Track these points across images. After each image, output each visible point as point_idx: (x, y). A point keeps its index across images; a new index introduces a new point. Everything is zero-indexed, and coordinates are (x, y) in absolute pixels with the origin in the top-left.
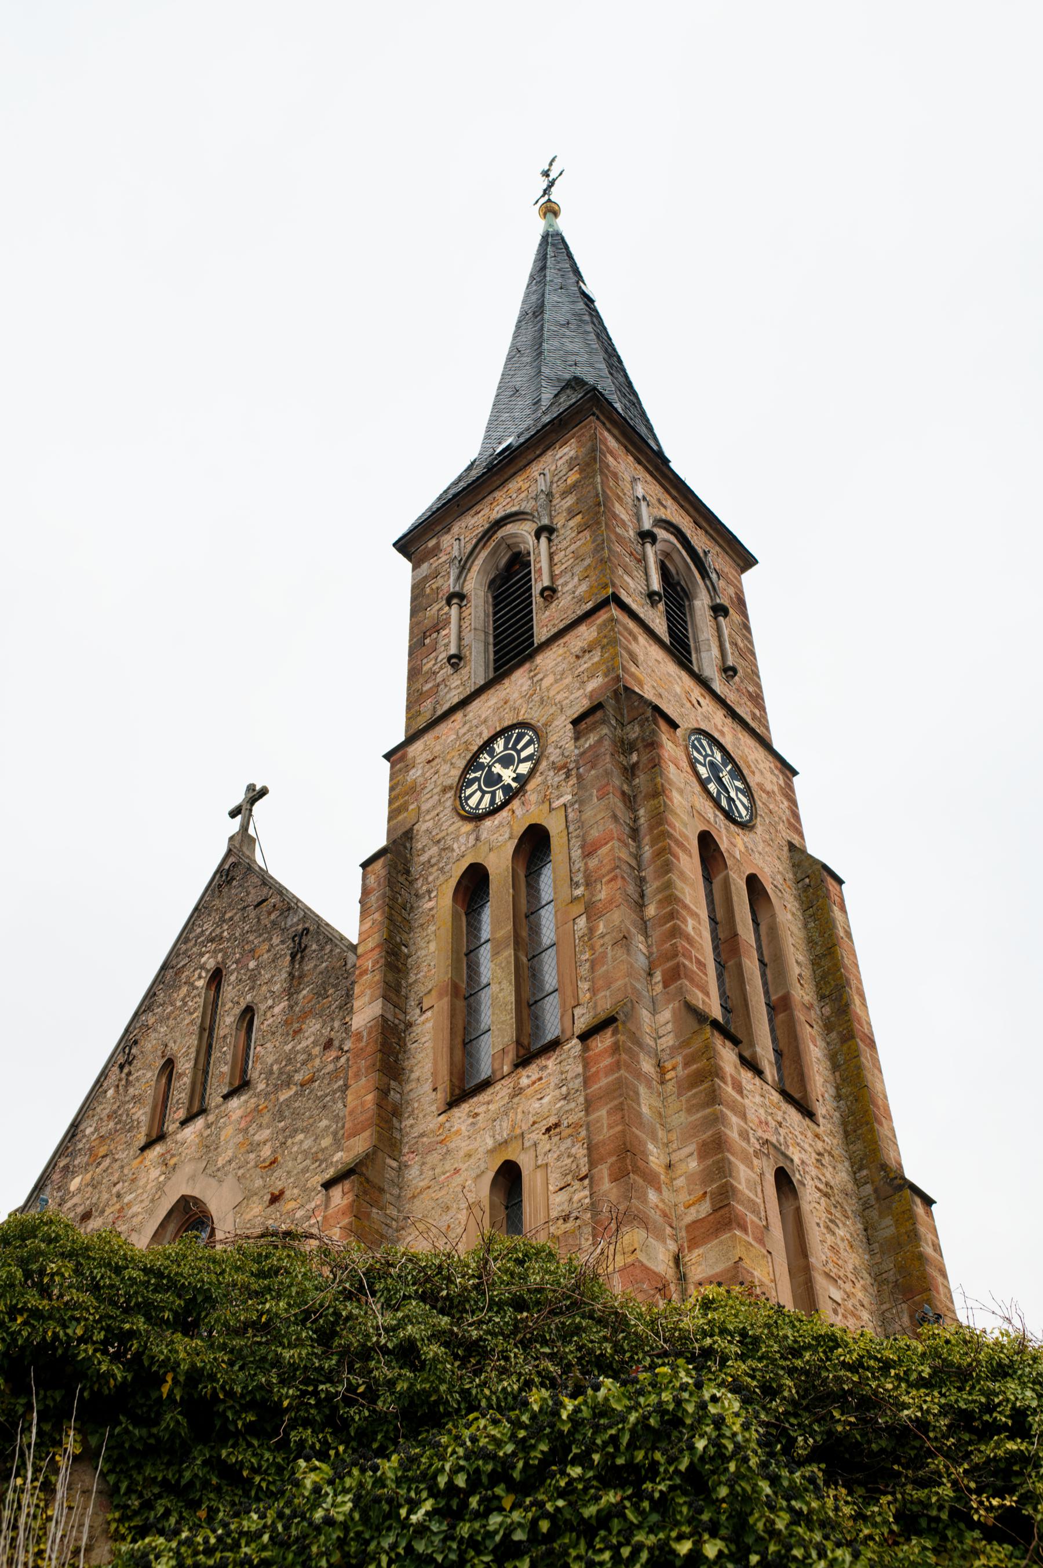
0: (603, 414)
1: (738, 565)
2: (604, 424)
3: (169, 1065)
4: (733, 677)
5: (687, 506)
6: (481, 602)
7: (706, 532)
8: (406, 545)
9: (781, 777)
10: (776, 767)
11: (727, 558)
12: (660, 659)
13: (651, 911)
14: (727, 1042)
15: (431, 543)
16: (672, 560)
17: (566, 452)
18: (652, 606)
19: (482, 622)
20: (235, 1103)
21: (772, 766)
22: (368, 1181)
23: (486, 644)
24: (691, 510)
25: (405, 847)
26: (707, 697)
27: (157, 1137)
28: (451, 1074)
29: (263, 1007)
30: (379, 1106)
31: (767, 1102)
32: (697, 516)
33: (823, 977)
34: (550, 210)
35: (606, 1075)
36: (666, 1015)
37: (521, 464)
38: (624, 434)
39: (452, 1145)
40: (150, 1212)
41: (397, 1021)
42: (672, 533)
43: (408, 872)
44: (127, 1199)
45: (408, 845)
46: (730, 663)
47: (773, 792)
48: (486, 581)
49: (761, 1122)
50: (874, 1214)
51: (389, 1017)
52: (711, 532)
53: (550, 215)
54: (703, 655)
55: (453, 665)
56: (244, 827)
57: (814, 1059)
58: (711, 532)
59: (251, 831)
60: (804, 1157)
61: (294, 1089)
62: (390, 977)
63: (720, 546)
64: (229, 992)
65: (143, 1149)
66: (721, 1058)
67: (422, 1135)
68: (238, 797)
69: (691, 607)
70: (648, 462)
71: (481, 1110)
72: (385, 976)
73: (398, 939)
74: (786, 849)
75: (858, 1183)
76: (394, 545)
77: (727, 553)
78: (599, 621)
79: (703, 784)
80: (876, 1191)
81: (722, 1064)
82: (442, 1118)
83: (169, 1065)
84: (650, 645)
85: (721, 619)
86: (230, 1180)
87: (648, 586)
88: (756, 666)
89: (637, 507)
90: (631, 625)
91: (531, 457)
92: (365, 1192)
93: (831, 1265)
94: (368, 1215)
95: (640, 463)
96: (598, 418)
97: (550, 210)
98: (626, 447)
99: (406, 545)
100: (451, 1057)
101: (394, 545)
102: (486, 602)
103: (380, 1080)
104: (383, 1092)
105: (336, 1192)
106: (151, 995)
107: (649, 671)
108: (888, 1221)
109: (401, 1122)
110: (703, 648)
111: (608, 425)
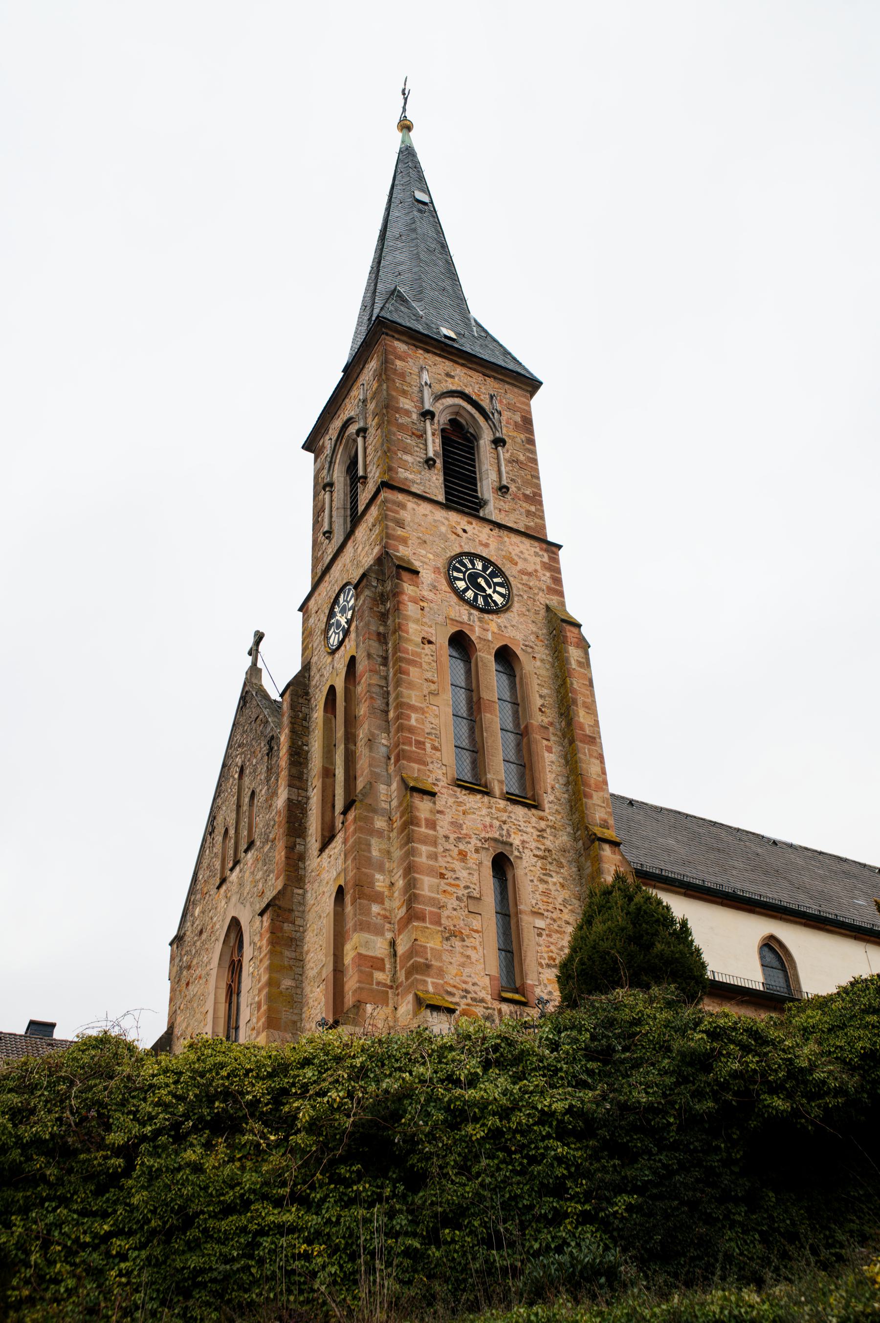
0: (391, 330)
1: (527, 391)
2: (393, 337)
3: (226, 831)
4: (506, 493)
5: (474, 366)
6: (342, 485)
7: (495, 378)
8: (308, 446)
9: (546, 555)
10: (541, 549)
11: (516, 390)
12: (427, 512)
13: (391, 715)
14: (425, 797)
15: (321, 443)
16: (461, 416)
17: (373, 365)
18: (430, 469)
19: (342, 502)
20: (249, 855)
21: (538, 550)
22: (280, 908)
23: (345, 517)
24: (479, 368)
25: (305, 677)
26: (474, 522)
27: (223, 881)
28: (323, 829)
29: (258, 790)
30: (287, 858)
31: (493, 811)
32: (484, 370)
33: (562, 701)
34: (405, 126)
35: (352, 836)
36: (394, 786)
37: (355, 377)
38: (411, 337)
39: (322, 877)
40: (222, 927)
41: (300, 798)
42: (457, 397)
43: (307, 694)
44: (215, 919)
45: (307, 675)
46: (504, 482)
47: (536, 571)
48: (344, 469)
49: (485, 827)
50: (583, 859)
51: (294, 797)
52: (499, 376)
53: (405, 130)
54: (484, 482)
55: (327, 538)
56: (254, 663)
57: (547, 763)
58: (499, 376)
59: (260, 664)
60: (525, 837)
61: (270, 844)
62: (294, 771)
63: (509, 383)
64: (247, 780)
65: (219, 888)
66: (418, 810)
67: (312, 871)
68: (250, 642)
69: (478, 446)
70: (435, 348)
71: (331, 853)
72: (290, 771)
73: (300, 743)
74: (543, 612)
75: (576, 840)
76: (303, 448)
77: (516, 386)
78: (378, 503)
79: (460, 595)
80: (584, 844)
81: (418, 814)
82: (319, 859)
83: (226, 831)
84: (419, 505)
85: (500, 448)
86: (248, 905)
87: (426, 454)
88: (537, 470)
89: (421, 391)
90: (400, 497)
91: (358, 371)
92: (278, 916)
93: (540, 905)
94: (281, 929)
95: (428, 351)
96: (387, 334)
97: (405, 126)
98: (414, 345)
99: (308, 446)
100: (322, 819)
101: (303, 448)
102: (345, 485)
103: (287, 841)
104: (290, 848)
105: (265, 918)
106: (219, 785)
107: (416, 527)
108: (589, 864)
109: (304, 863)
110: (484, 478)
111: (396, 336)
